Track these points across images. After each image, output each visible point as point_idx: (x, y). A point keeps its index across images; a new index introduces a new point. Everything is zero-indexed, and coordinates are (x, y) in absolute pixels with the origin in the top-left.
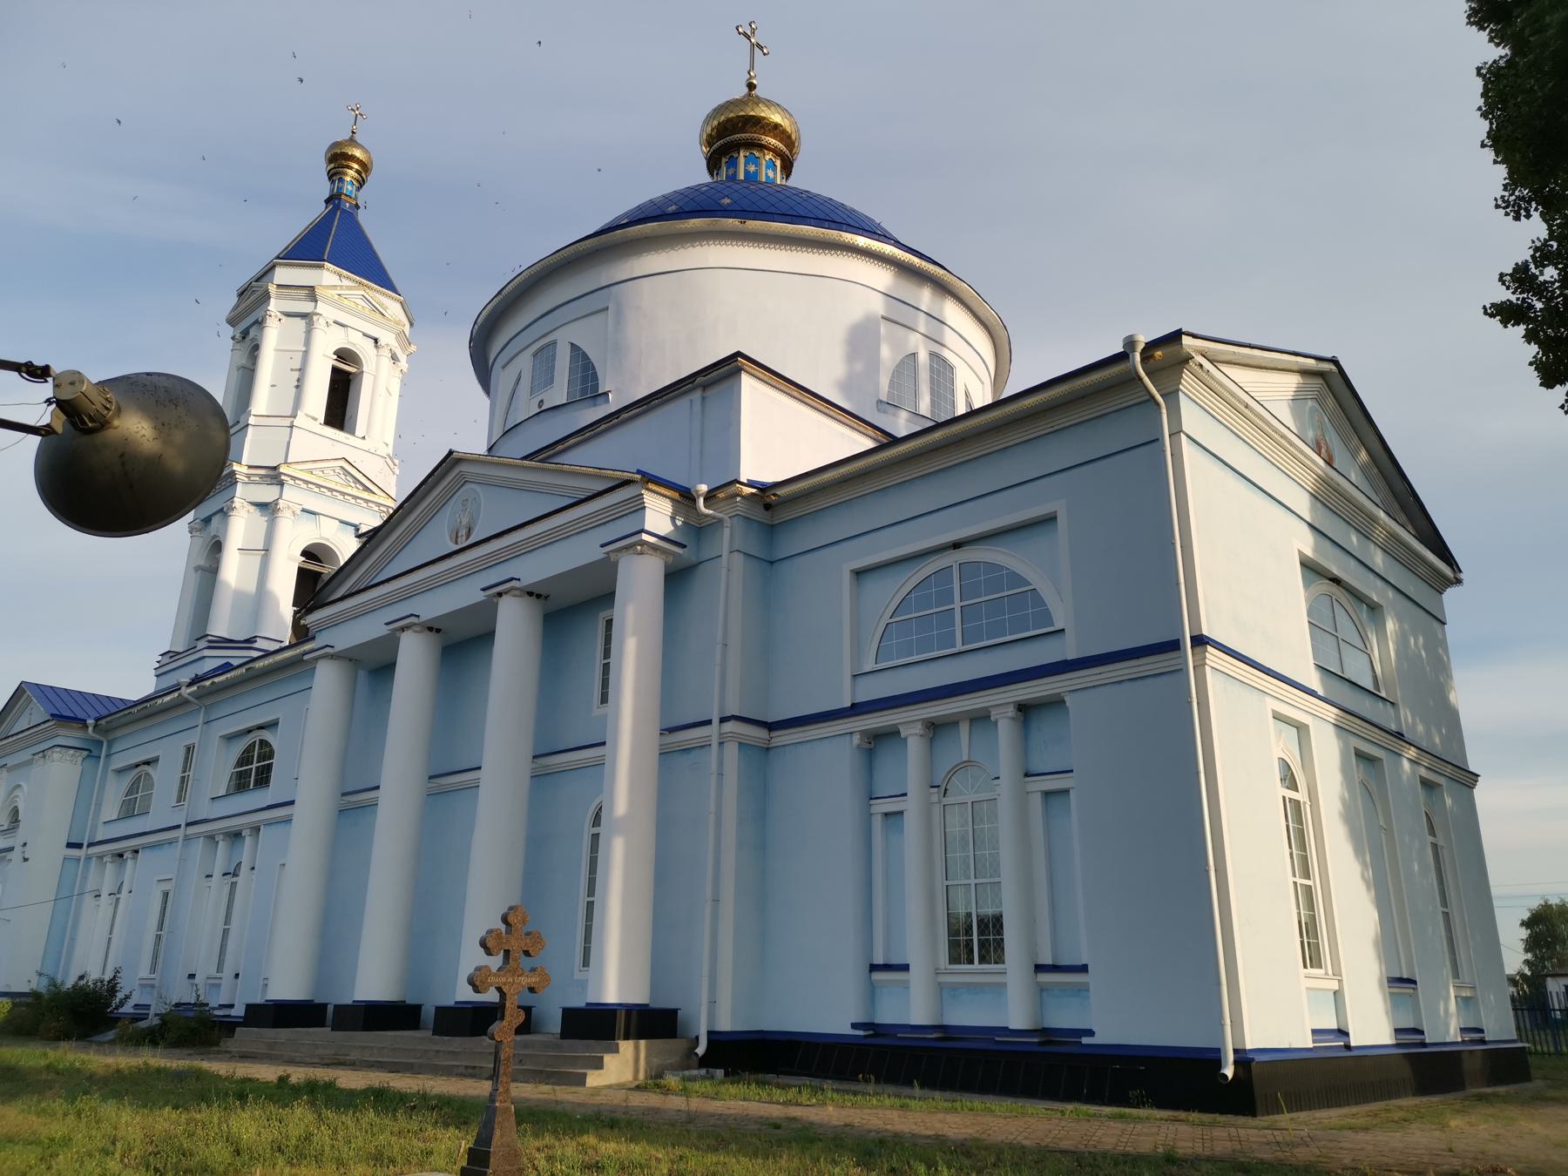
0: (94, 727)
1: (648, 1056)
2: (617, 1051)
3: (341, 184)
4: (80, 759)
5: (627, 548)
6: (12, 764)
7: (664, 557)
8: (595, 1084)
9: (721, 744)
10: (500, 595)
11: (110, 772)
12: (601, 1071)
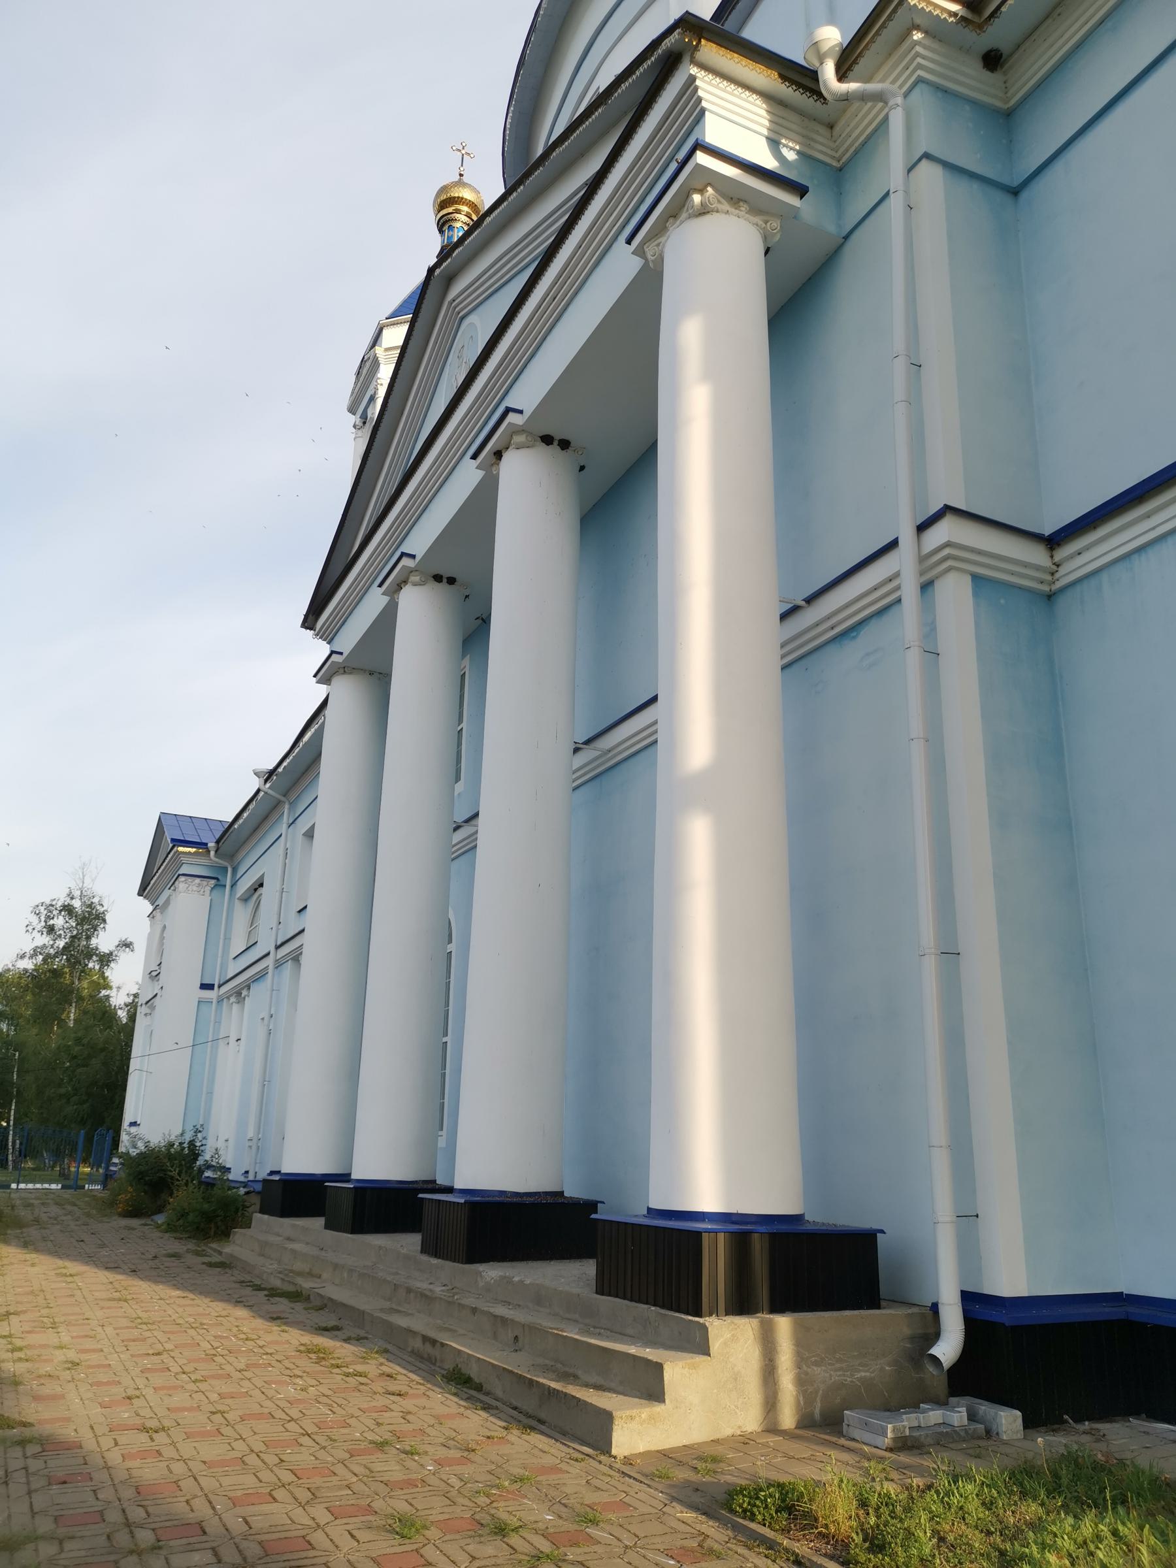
0: (216, 852)
1: (801, 1360)
2: (703, 1348)
3: (451, 233)
4: (208, 889)
5: (673, 214)
6: (162, 902)
7: (758, 220)
8: (642, 1445)
9: (926, 587)
10: (498, 455)
11: (236, 900)
12: (658, 1408)
